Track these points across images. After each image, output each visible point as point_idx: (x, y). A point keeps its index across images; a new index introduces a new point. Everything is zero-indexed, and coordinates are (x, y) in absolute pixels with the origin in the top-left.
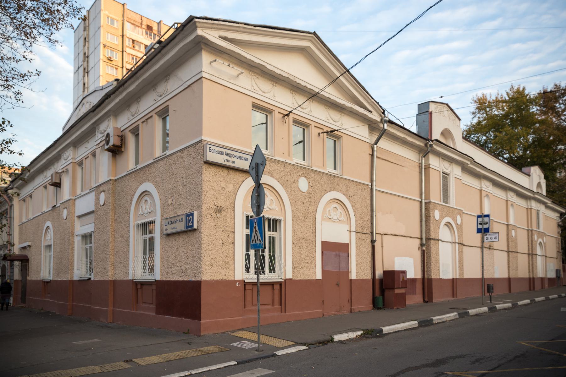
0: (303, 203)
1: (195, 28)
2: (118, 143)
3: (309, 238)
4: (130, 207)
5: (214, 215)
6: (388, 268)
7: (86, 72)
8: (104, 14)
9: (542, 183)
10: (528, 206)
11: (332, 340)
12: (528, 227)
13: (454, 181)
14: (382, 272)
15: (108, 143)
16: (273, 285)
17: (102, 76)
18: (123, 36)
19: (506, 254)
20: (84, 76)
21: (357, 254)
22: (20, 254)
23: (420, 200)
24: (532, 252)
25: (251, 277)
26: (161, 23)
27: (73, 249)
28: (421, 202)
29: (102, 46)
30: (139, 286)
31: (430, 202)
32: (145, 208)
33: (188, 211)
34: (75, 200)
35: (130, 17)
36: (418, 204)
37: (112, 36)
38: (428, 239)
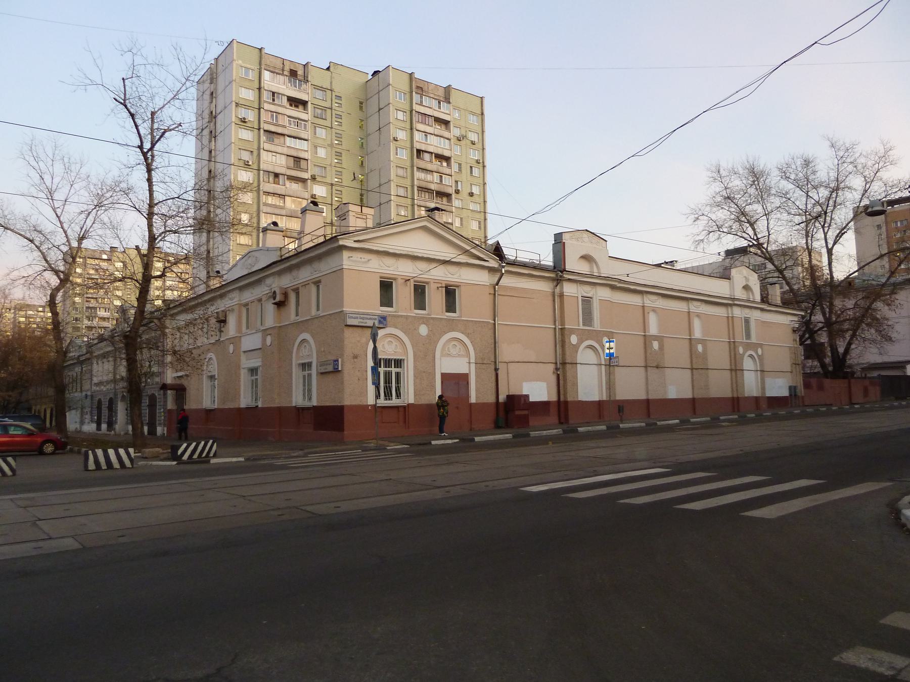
0: (424, 344)
1: (338, 240)
2: (283, 299)
3: (429, 371)
4: (293, 349)
5: (352, 360)
6: (514, 391)
7: (213, 135)
8: (237, 64)
9: (751, 284)
10: (728, 314)
11: (431, 443)
12: (729, 339)
13: (598, 303)
14: (505, 396)
15: (274, 298)
16: (398, 408)
17: (234, 143)
18: (259, 89)
19: (689, 372)
20: (210, 141)
21: (477, 381)
22: (173, 383)
23: (554, 327)
24: (736, 366)
25: (382, 402)
26: (308, 66)
27: (239, 381)
28: (555, 328)
29: (234, 104)
30: (301, 411)
31: (565, 328)
32: (304, 351)
33: (334, 358)
34: (241, 337)
35: (268, 63)
36: (552, 332)
37: (247, 90)
38: (564, 364)
